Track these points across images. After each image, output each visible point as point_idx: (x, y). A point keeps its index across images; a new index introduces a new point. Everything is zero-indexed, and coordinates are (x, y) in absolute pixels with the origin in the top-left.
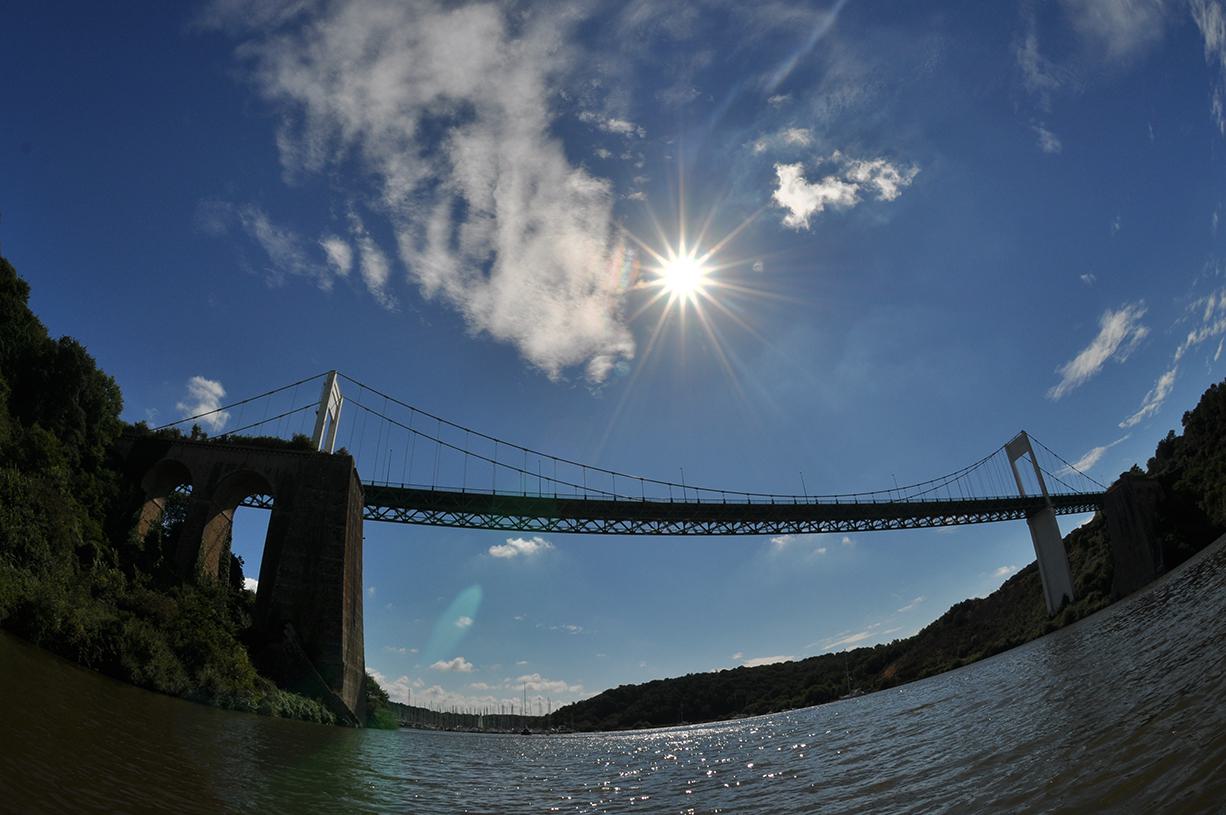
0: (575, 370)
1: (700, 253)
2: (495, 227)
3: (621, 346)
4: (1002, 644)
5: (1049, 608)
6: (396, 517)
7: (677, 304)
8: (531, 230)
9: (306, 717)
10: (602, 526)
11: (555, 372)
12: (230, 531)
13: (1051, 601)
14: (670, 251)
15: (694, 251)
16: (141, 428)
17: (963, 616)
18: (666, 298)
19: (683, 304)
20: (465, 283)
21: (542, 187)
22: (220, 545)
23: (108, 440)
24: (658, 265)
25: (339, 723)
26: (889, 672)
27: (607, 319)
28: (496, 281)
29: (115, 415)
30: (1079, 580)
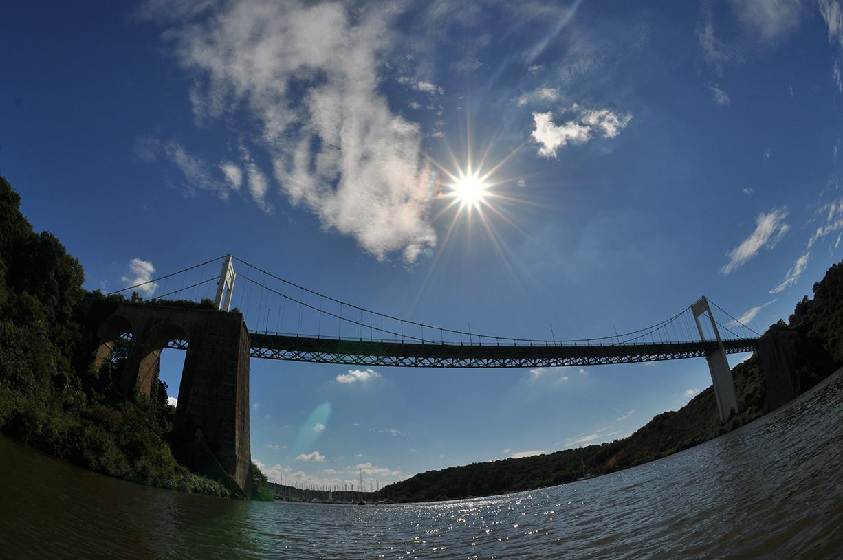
0: (396, 254)
1: (481, 174)
2: (341, 156)
3: (427, 238)
4: (689, 443)
5: (721, 418)
6: (272, 355)
7: (465, 209)
8: (365, 158)
9: (210, 493)
10: (414, 361)
11: (381, 256)
12: (158, 365)
13: (723, 413)
14: (461, 172)
15: (477, 173)
16: (97, 294)
17: (662, 423)
18: (458, 205)
19: (469, 209)
20: (320, 195)
21: (373, 129)
22: (151, 375)
23: (74, 302)
24: (452, 182)
25: (233, 497)
26: (611, 462)
27: (417, 220)
28: (341, 193)
29: (79, 285)
30: (742, 398)
